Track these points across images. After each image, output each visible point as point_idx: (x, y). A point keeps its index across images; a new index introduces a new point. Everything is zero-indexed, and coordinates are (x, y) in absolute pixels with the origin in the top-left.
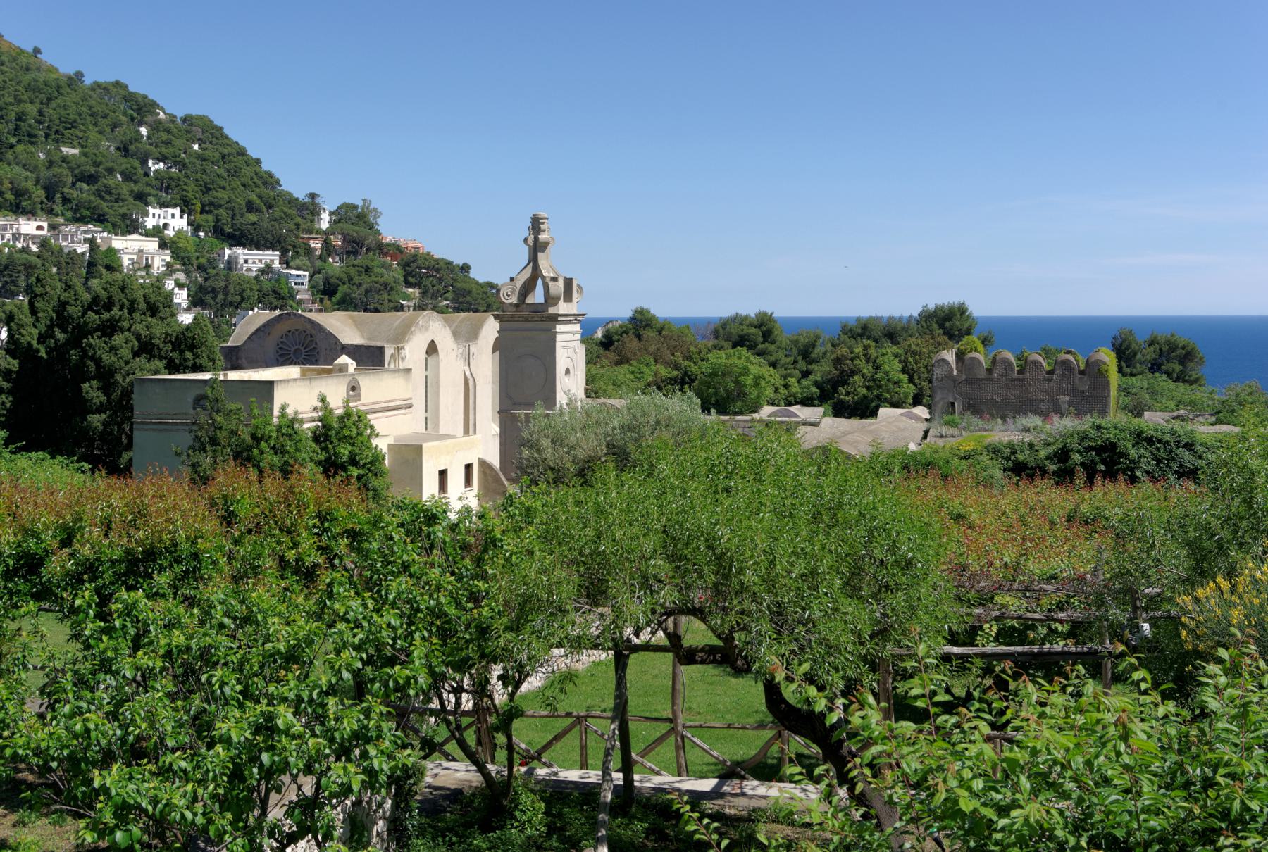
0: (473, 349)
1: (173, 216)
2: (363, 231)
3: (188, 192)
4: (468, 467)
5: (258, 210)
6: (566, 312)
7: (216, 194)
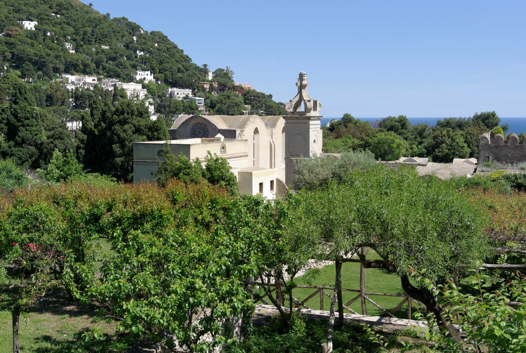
1: (147, 75)
2: (227, 80)
3: (153, 64)
4: (272, 182)
5: (183, 72)
7: (165, 65)
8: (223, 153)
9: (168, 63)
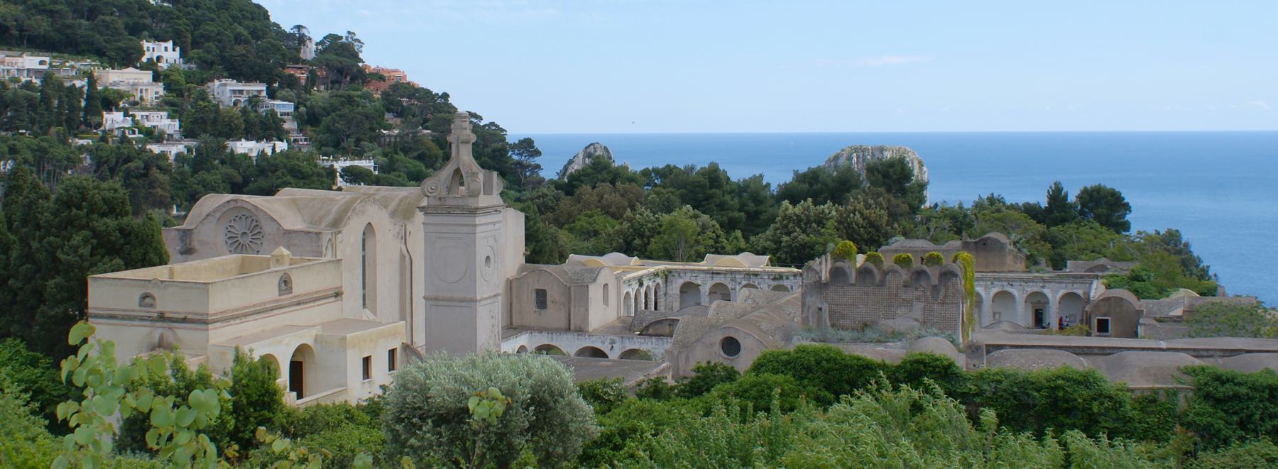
0: (409, 228)
1: (166, 49)
2: (348, 61)
3: (180, 25)
4: (392, 353)
5: (247, 42)
6: (486, 205)
7: (207, 27)
8: (284, 294)
9: (213, 20)
